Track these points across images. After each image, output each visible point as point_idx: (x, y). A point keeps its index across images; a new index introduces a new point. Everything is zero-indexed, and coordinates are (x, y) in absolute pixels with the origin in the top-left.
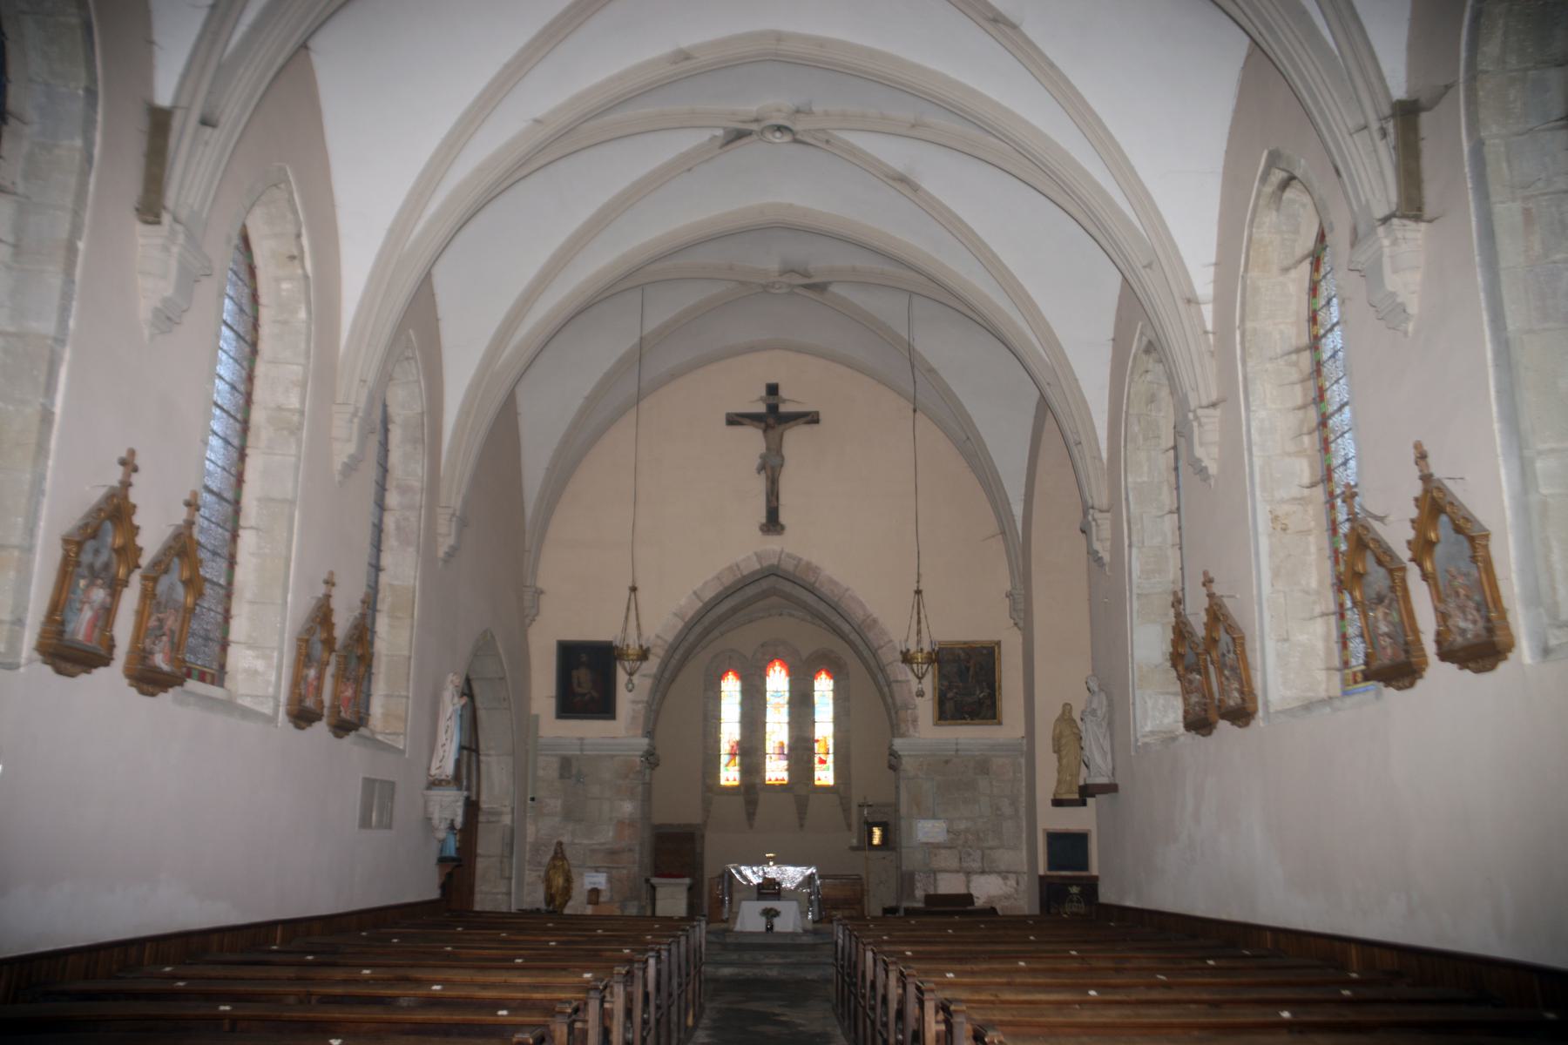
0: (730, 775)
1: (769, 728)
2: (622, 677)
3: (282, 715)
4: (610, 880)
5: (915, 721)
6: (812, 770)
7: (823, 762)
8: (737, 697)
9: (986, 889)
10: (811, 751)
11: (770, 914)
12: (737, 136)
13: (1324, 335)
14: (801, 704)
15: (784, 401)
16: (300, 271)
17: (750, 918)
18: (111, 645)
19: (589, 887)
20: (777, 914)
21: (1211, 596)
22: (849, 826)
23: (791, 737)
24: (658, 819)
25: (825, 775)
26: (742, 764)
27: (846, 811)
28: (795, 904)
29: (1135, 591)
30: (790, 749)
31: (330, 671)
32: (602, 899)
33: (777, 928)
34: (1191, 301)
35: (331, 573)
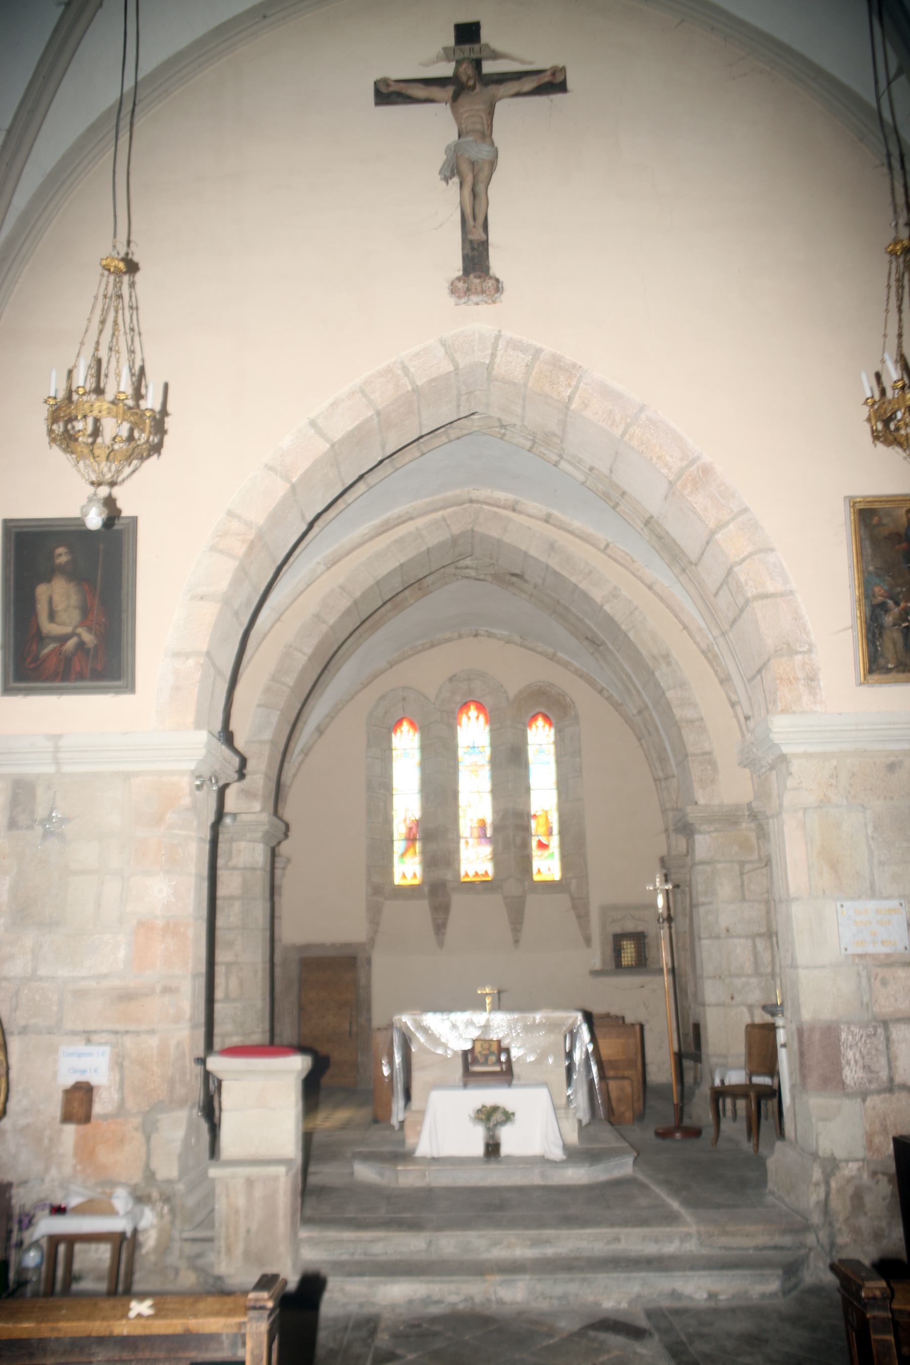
0: (407, 869)
4: (118, 1063)
5: (811, 678)
7: (542, 846)
11: (493, 1118)
14: (510, 760)
15: (495, 56)
19: (69, 1080)
20: (508, 1117)
22: (588, 941)
23: (495, 811)
24: (292, 933)
25: (547, 866)
26: (424, 853)
27: (582, 916)
28: (543, 1093)
30: (497, 828)
32: (98, 1108)
33: (506, 1149)
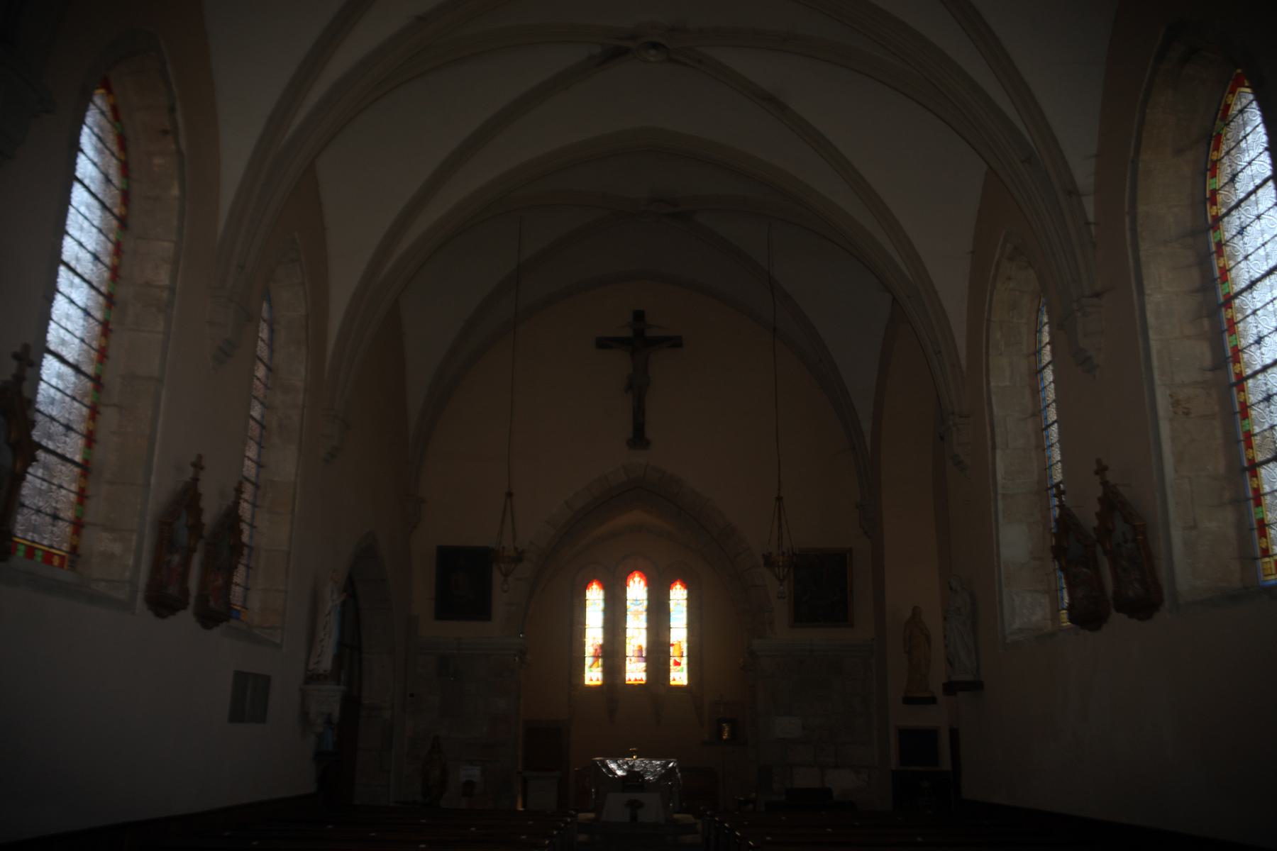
1: (629, 633)
2: (497, 578)
3: (140, 603)
6: (668, 671)
7: (677, 664)
8: (601, 605)
9: (841, 782)
10: (667, 656)
11: (634, 806)
12: (615, 54)
13: (1228, 213)
16: (173, 147)
17: (615, 809)
18: (185, 592)
21: (1105, 484)
23: (649, 642)
25: (679, 676)
29: (1000, 491)
30: (648, 650)
31: (197, 559)
34: (1073, 192)
35: (200, 457)
